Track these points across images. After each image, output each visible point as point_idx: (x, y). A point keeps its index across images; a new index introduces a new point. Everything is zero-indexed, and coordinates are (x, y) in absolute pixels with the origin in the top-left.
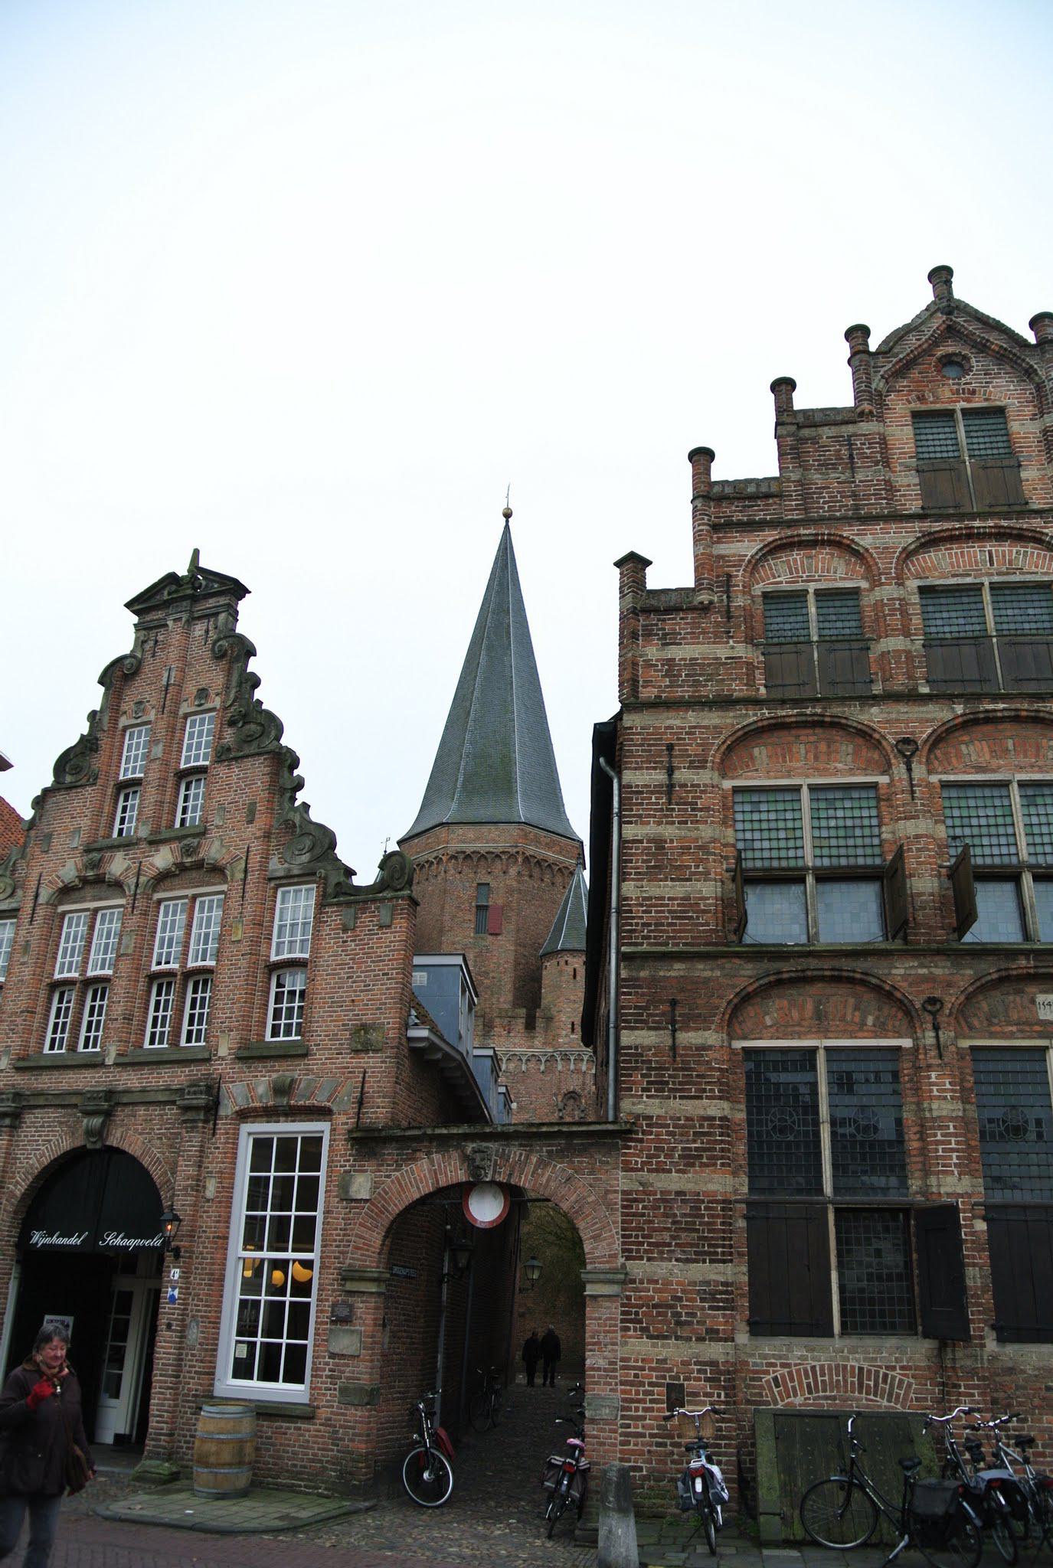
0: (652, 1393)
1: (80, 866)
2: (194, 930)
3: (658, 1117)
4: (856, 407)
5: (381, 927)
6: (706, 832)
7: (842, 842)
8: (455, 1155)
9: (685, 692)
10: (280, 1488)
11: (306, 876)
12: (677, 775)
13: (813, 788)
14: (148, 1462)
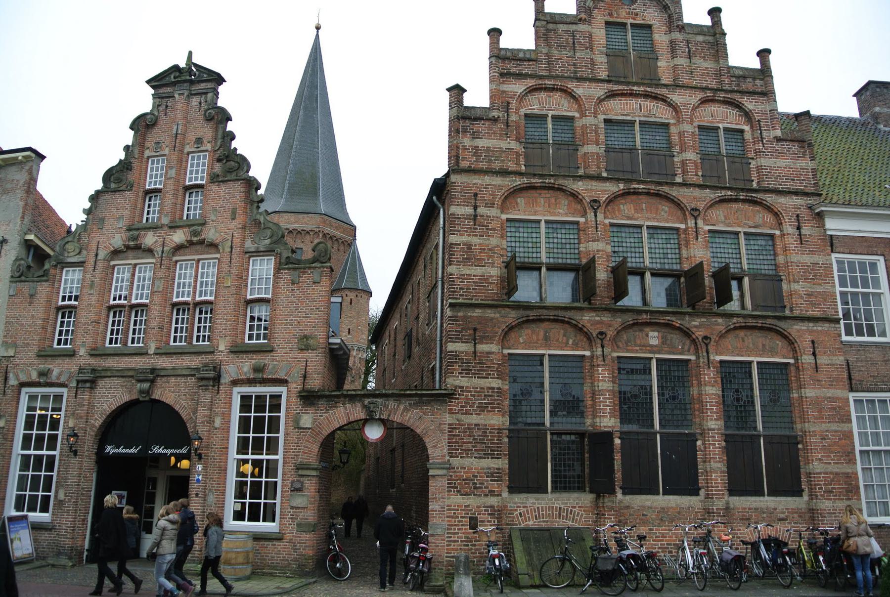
0: (462, 521)
1: (124, 238)
2: (199, 279)
3: (467, 387)
4: (577, 15)
5: (314, 283)
6: (494, 241)
7: (560, 251)
8: (359, 405)
9: (483, 165)
10: (264, 574)
11: (269, 251)
12: (479, 210)
13: (547, 222)
14: (188, 565)
